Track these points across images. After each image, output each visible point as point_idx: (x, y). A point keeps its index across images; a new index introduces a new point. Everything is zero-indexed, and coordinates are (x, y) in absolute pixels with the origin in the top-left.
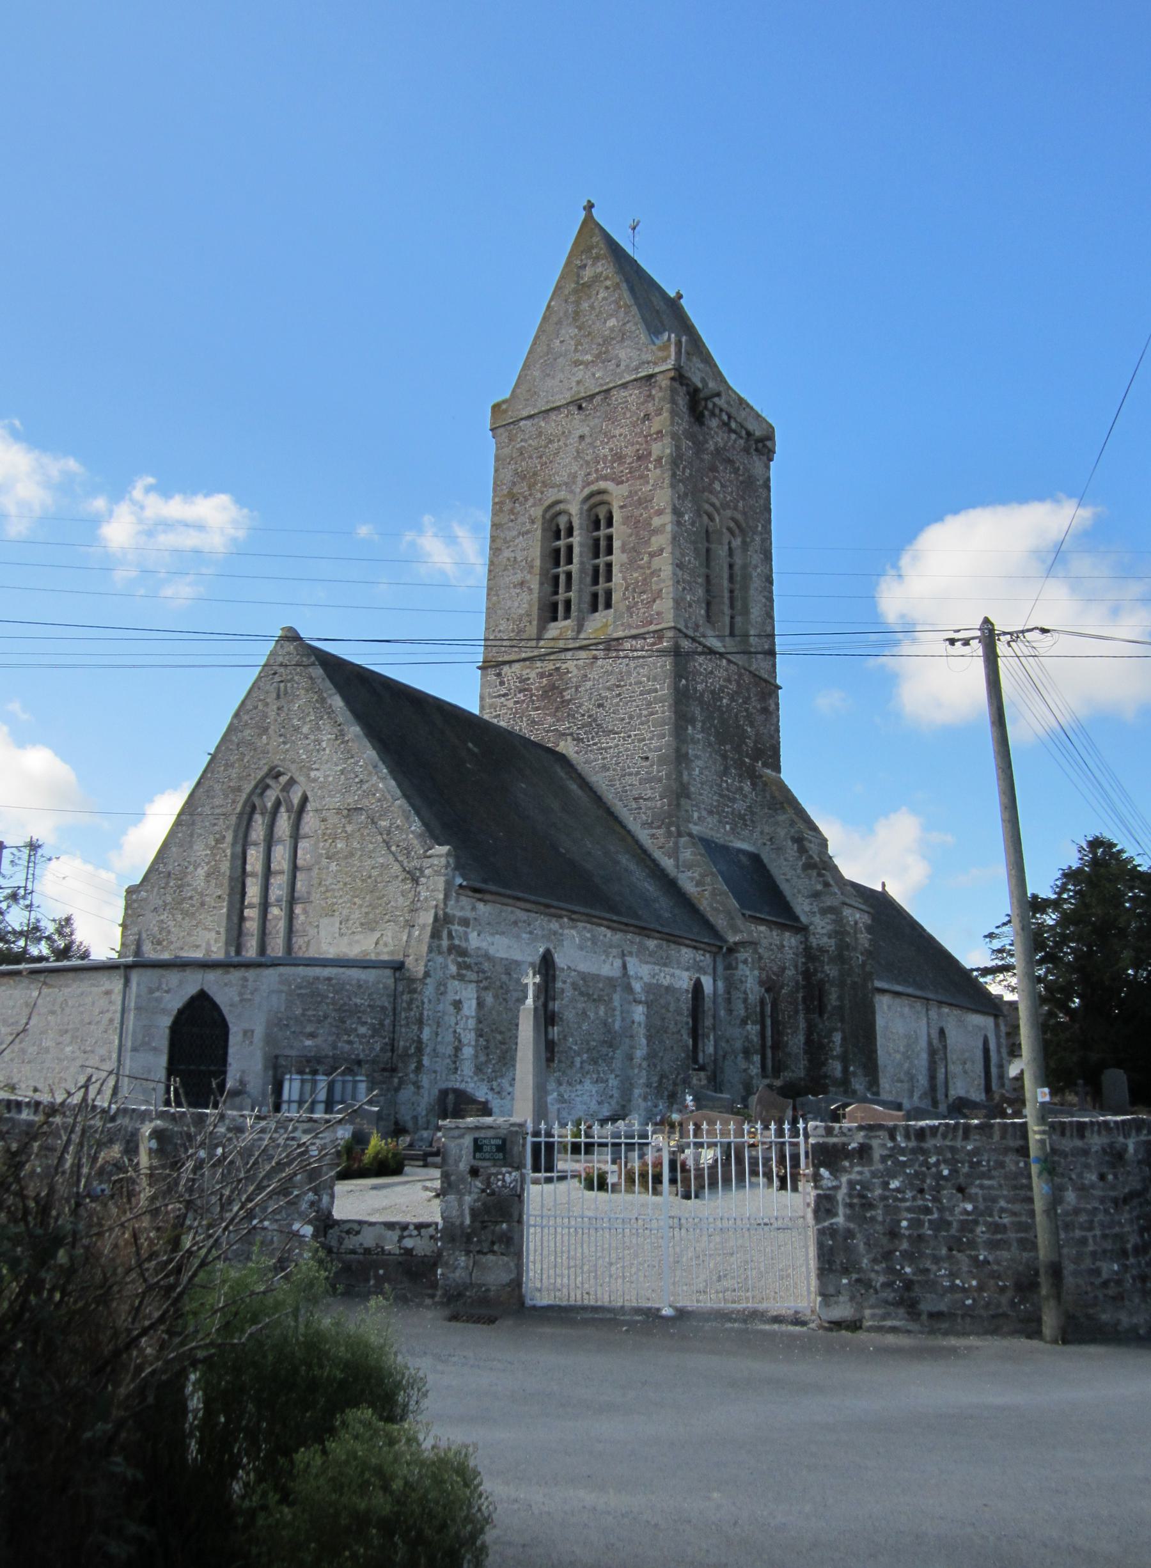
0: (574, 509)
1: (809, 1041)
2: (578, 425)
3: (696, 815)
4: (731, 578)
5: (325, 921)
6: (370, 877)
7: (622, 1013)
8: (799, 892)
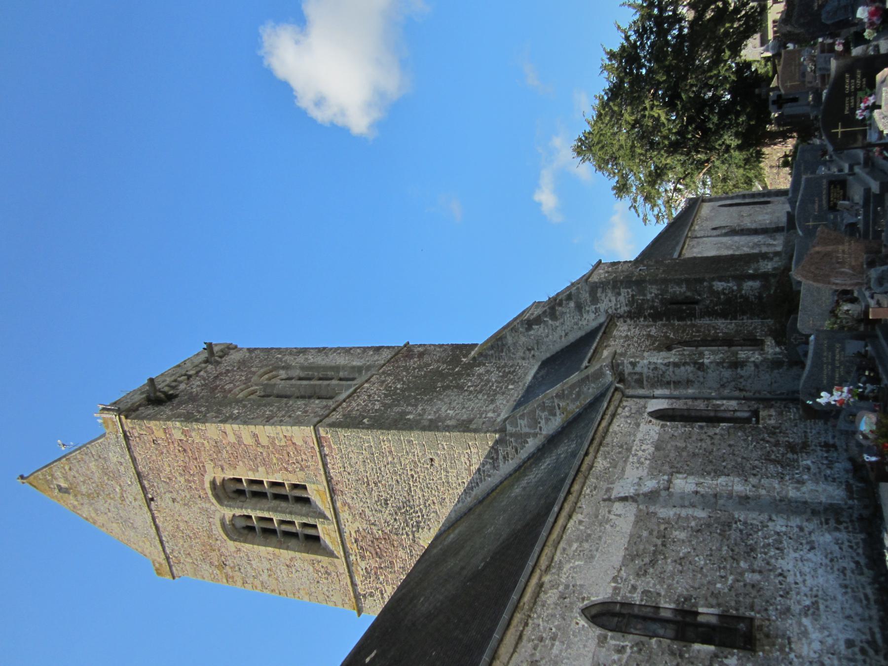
0: (228, 513)
1: (724, 315)
2: (163, 503)
3: (490, 415)
4: (309, 379)
7: (683, 506)
8: (576, 324)
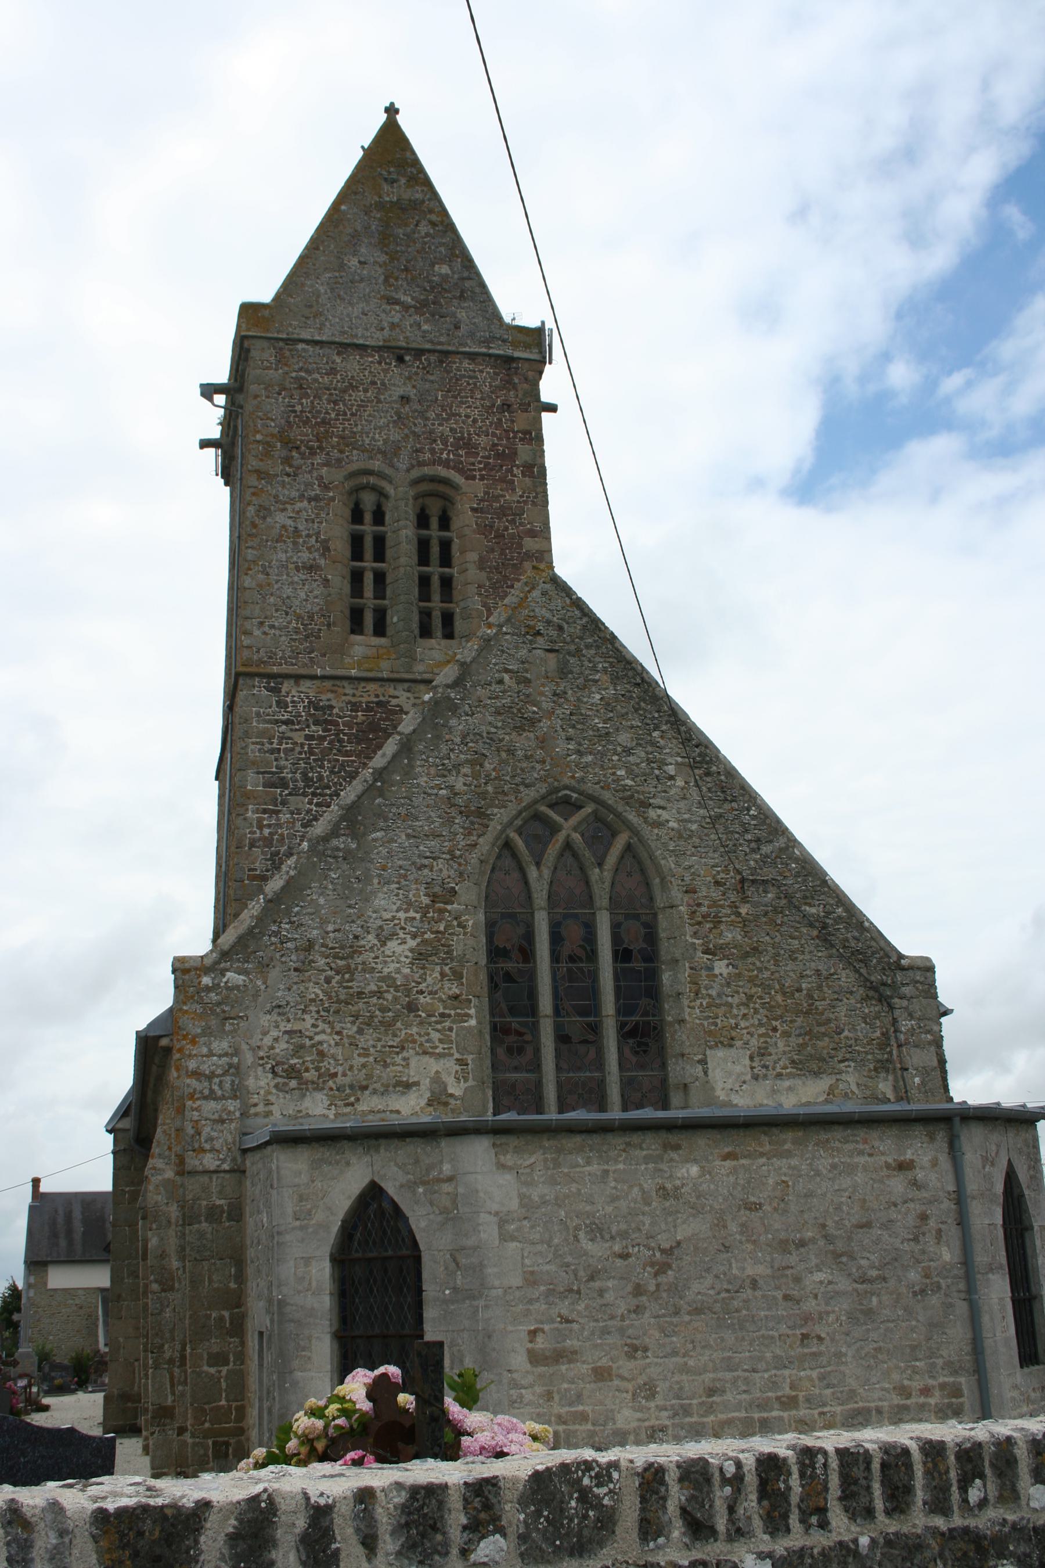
5: (717, 1056)
6: (799, 990)
